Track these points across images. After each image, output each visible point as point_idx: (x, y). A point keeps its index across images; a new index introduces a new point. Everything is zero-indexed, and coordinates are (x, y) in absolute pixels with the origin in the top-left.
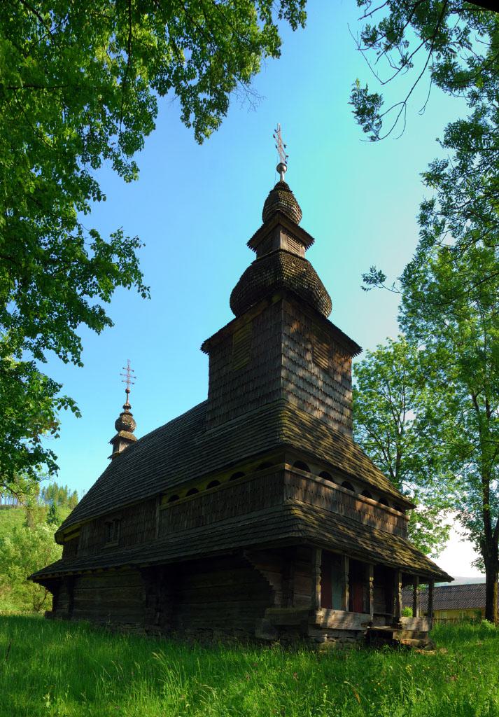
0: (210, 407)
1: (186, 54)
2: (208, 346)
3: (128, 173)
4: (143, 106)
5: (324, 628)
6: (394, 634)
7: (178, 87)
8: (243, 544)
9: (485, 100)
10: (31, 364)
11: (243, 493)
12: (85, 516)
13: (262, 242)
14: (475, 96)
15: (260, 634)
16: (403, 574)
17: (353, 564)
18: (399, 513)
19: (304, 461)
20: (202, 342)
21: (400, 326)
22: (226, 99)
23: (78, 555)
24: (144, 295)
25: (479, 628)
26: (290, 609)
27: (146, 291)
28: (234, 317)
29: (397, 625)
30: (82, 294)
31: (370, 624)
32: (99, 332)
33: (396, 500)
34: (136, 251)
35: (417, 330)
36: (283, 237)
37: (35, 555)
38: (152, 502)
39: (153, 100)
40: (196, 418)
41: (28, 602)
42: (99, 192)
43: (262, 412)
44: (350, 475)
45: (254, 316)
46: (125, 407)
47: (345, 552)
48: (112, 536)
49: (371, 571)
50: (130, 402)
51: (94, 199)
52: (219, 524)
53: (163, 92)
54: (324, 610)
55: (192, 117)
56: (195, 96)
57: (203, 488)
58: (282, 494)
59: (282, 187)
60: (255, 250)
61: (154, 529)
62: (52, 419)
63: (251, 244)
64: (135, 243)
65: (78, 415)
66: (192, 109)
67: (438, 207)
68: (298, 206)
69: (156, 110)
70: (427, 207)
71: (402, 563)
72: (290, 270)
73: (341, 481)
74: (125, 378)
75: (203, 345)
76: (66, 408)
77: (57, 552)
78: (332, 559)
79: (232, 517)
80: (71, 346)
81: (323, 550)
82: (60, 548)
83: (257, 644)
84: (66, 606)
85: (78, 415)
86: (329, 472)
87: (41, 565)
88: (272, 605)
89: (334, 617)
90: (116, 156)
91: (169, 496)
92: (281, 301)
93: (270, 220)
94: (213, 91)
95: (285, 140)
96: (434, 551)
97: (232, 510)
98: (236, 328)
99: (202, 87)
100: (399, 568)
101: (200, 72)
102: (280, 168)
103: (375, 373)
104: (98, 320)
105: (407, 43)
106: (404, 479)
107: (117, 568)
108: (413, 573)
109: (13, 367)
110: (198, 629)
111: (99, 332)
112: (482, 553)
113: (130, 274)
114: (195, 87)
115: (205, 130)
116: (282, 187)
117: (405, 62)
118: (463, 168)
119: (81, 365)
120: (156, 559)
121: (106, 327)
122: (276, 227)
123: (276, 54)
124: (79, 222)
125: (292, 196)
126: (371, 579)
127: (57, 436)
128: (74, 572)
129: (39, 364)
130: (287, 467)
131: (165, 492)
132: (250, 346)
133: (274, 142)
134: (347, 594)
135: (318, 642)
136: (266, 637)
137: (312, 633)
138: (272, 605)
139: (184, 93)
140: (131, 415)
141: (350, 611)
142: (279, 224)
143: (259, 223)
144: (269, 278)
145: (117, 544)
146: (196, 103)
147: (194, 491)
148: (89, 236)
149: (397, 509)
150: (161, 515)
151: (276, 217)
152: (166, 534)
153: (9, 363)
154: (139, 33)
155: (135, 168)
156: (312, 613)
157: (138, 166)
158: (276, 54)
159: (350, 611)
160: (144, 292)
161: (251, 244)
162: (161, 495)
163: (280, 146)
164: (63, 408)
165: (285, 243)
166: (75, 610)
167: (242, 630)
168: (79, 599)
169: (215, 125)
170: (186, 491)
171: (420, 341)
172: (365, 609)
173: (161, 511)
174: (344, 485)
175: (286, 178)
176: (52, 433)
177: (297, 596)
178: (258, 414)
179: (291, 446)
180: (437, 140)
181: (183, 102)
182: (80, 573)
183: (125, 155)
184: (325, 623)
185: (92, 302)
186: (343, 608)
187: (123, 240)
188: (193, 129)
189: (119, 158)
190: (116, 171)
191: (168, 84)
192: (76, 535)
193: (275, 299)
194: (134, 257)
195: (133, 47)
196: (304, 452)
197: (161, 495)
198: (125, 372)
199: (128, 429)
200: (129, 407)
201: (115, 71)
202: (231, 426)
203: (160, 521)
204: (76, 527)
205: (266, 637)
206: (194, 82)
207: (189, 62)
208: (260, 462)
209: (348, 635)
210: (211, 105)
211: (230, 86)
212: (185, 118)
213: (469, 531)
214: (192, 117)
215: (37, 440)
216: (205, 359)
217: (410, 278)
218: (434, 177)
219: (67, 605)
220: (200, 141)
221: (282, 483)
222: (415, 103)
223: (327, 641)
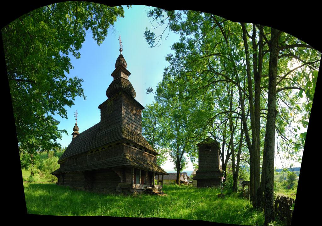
0: (101, 125)
1: (94, 16)
2: (100, 107)
3: (77, 56)
4: (81, 34)
5: (135, 189)
6: (153, 190)
7: (92, 27)
8: (112, 166)
9: (185, 35)
10: (51, 116)
12: (66, 157)
13: (115, 74)
14: (182, 34)
15: (117, 190)
17: (142, 171)
18: (155, 156)
19: (129, 142)
20: (98, 106)
21: (155, 99)
22: (107, 31)
24: (84, 99)
25: (174, 186)
26: (126, 184)
27: (85, 98)
28: (107, 98)
29: (153, 186)
30: (66, 97)
31: (147, 187)
32: (70, 107)
34: (81, 83)
35: (160, 100)
36: (122, 73)
37: (52, 166)
38: (85, 153)
39: (84, 31)
40: (96, 128)
41: (50, 179)
42: (71, 66)
43: (117, 127)
44: (141, 146)
45: (113, 98)
46: (76, 124)
49: (147, 173)
50: (77, 123)
51: (70, 68)
53: (87, 29)
54: (135, 184)
55: (96, 36)
56: (97, 30)
57: (100, 149)
58: (123, 152)
59: (121, 56)
60: (113, 77)
61: (86, 161)
62: (60, 135)
63: (112, 75)
64: (81, 80)
65: (67, 135)
66: (96, 34)
67: (169, 70)
68: (126, 63)
69: (85, 34)
70: (166, 69)
71: (155, 170)
72: (124, 84)
73: (139, 148)
74: (75, 116)
76: (64, 132)
77: (58, 166)
78: (137, 170)
80: (63, 113)
82: (59, 165)
83: (117, 194)
85: (67, 135)
86: (136, 145)
87: (54, 170)
88: (120, 182)
89: (137, 186)
90: (73, 51)
91: (90, 152)
94: (102, 28)
95: (122, 40)
96: (163, 163)
99: (99, 27)
101: (98, 22)
102: (120, 50)
103: (148, 112)
104: (70, 104)
105: (163, 16)
106: (155, 144)
107: (76, 172)
109: (46, 117)
111: (70, 107)
112: (176, 165)
113: (81, 92)
114: (97, 27)
115: (100, 41)
116: (121, 56)
117: (162, 22)
118: (177, 57)
119: (67, 118)
120: (87, 170)
121: (72, 106)
122: (120, 70)
123: (123, 16)
124: (66, 76)
125: (124, 59)
126: (147, 175)
127: (61, 140)
129: (53, 116)
130: (125, 144)
133: (119, 41)
134: (141, 180)
135: (133, 193)
136: (119, 191)
137: (131, 190)
138: (120, 182)
139: (93, 29)
140: (77, 126)
142: (120, 69)
143: (115, 69)
144: (118, 86)
146: (97, 32)
147: (97, 150)
149: (154, 155)
150: (88, 157)
151: (120, 67)
153: (45, 116)
154: (79, 9)
155: (79, 54)
156: (132, 185)
157: (80, 53)
158: (123, 16)
160: (85, 98)
161: (112, 75)
162: (88, 151)
163: (120, 43)
164: (63, 133)
165: (122, 75)
169: (103, 39)
171: (161, 103)
172: (145, 182)
173: (88, 156)
174: (140, 149)
176: (60, 139)
177: (127, 180)
179: (126, 139)
180: (170, 47)
181: (93, 32)
183: (76, 50)
184: (135, 188)
185: (69, 99)
186: (139, 183)
187: (77, 79)
188: (96, 41)
189: (74, 51)
190: (74, 56)
191: (89, 26)
192: (64, 161)
193: (120, 93)
194: (80, 84)
195: (77, 14)
196: (129, 140)
197: (88, 151)
198: (75, 114)
199: (77, 130)
200: (77, 124)
201: (72, 23)
204: (64, 159)
205: (119, 191)
206: (96, 25)
207: (95, 18)
209: (140, 190)
210: (102, 33)
211: (107, 26)
212: (94, 37)
213: (173, 159)
214: (96, 36)
215: (55, 141)
216: (99, 110)
217: (159, 91)
218: (168, 59)
220: (99, 45)
221: (123, 149)
222: (164, 36)
223: (135, 193)
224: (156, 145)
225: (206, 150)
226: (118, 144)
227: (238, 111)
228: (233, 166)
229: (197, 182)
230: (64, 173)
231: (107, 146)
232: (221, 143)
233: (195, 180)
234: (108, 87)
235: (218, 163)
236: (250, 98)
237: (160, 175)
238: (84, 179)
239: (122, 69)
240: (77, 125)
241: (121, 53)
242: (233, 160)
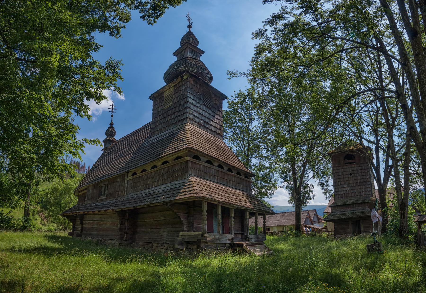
2: (153, 97)
11: (168, 172)
16: (249, 212)
23: (86, 202)
33: (245, 172)
38: (123, 176)
45: (174, 84)
47: (219, 203)
48: (103, 193)
52: (156, 188)
59: (190, 34)
61: (124, 190)
75: (150, 96)
79: (162, 184)
81: (208, 203)
92: (188, 78)
93: (184, 45)
97: (162, 180)
98: (166, 89)
100: (247, 209)
106: (252, 157)
108: (255, 212)
116: (190, 34)
128: (83, 212)
131: (131, 171)
140: (114, 128)
141: (223, 233)
145: (105, 197)
147: (144, 170)
148: (70, 162)
150: (127, 183)
152: (130, 193)
159: (223, 233)
163: (189, 20)
166: (83, 232)
167: (168, 243)
168: (86, 226)
170: (141, 170)
178: (175, 130)
182: (86, 213)
192: (85, 191)
193: (185, 77)
202: (163, 135)
203: (127, 186)
208: (176, 156)
224: (254, 159)
225: (346, 164)
226: (178, 158)
228: (398, 189)
229: (334, 226)
230: (84, 214)
232: (373, 147)
233: (331, 223)
234: (167, 68)
235: (372, 186)
236: (126, 165)
237: (259, 215)
238: (119, 225)
239: (189, 47)
240: (113, 126)
241: (190, 30)
242: (398, 181)
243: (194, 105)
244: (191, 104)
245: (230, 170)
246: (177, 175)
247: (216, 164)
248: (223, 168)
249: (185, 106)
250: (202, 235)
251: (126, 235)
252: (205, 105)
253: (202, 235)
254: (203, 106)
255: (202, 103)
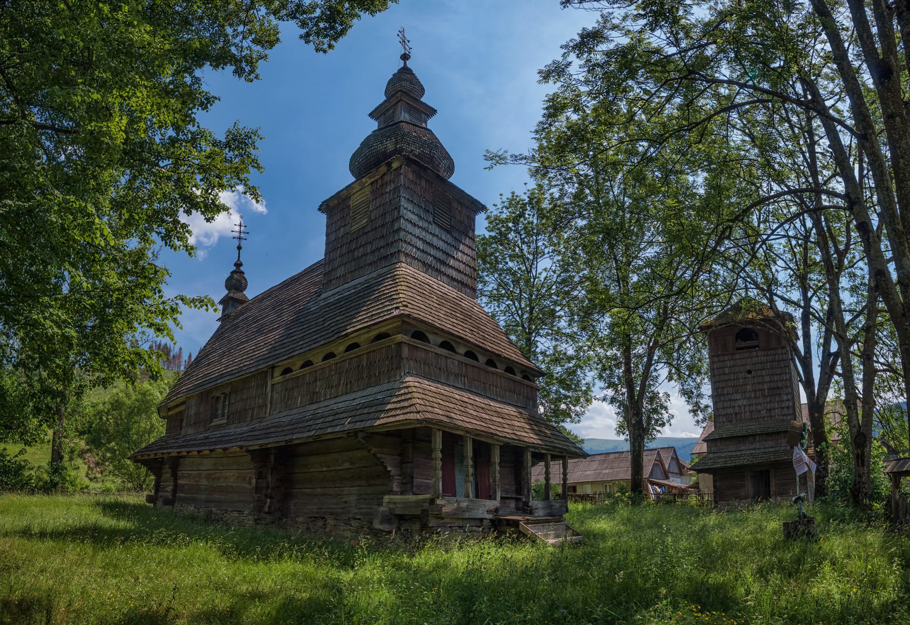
2: (326, 207)
11: (359, 366)
16: (532, 452)
23: (183, 432)
33: (523, 368)
38: (263, 375)
45: (372, 180)
47: (467, 432)
52: (333, 401)
59: (405, 71)
61: (266, 406)
75: (321, 206)
79: (347, 393)
81: (444, 432)
84: (170, 488)
92: (401, 166)
93: (392, 96)
97: (347, 385)
98: (355, 191)
100: (528, 447)
108: (544, 451)
110: (311, 518)
116: (405, 71)
132: (368, 207)
140: (243, 273)
141: (477, 497)
145: (225, 421)
150: (272, 391)
152: (277, 411)
159: (477, 497)
163: (404, 42)
166: (178, 495)
167: (359, 519)
168: (184, 482)
170: (300, 363)
175: (409, 64)
178: (375, 278)
182: (185, 454)
192: (182, 408)
193: (395, 165)
202: (349, 289)
203: (272, 397)
208: (377, 332)
219: (171, 487)
226: (380, 337)
227: (839, 186)
229: (715, 481)
231: (342, 348)
232: (798, 314)
233: (707, 475)
234: (357, 146)
235: (795, 397)
237: (554, 458)
238: (254, 481)
239: (405, 99)
240: (242, 268)
241: (405, 63)
243: (415, 225)
244: (407, 222)
245: (490, 363)
246: (379, 373)
247: (462, 350)
248: (476, 359)
249: (396, 226)
250: (432, 501)
251: (269, 500)
252: (438, 225)
253: (432, 501)
254: (434, 226)
255: (431, 219)
